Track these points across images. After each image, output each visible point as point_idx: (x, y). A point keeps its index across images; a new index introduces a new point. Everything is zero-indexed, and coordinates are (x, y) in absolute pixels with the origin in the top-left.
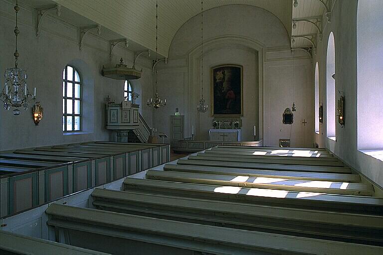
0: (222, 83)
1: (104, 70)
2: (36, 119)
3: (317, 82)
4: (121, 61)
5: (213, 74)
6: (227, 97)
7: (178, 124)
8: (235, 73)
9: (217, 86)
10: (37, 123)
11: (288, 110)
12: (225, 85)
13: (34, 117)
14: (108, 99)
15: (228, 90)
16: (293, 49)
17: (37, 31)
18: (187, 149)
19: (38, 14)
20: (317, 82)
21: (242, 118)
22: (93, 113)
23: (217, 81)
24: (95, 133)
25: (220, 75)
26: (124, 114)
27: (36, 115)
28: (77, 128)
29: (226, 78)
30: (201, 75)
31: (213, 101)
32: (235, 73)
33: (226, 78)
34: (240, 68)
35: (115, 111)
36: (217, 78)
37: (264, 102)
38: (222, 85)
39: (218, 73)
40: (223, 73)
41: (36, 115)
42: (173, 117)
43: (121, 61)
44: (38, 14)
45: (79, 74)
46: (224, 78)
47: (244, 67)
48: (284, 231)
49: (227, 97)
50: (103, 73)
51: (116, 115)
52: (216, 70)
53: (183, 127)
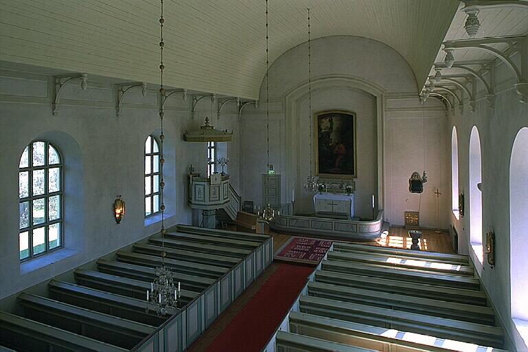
0: (328, 134)
1: (187, 136)
2: (117, 216)
3: (455, 145)
4: (207, 120)
5: (316, 122)
6: (335, 153)
7: (272, 186)
8: (346, 122)
9: (323, 138)
10: (118, 221)
11: (415, 174)
12: (333, 136)
13: (115, 214)
14: (191, 169)
15: (337, 144)
16: (421, 98)
17: (118, 111)
18: (288, 227)
19: (119, 91)
20: (455, 145)
21: (354, 180)
22: (173, 186)
23: (323, 131)
24: (176, 215)
25: (326, 123)
26: (212, 190)
27: (118, 211)
28: (156, 209)
29: (334, 128)
30: (312, 134)
31: (317, 156)
32: (346, 122)
33: (334, 128)
34: (352, 116)
35: (202, 187)
36: (323, 127)
37: (384, 160)
38: (329, 136)
39: (323, 120)
40: (331, 121)
41: (118, 211)
42: (266, 176)
43: (207, 120)
44: (119, 91)
45: (158, 143)
46: (331, 128)
47: (357, 114)
48: (380, 275)
49: (335, 153)
50: (185, 138)
51: (202, 191)
52: (321, 117)
53: (279, 190)
